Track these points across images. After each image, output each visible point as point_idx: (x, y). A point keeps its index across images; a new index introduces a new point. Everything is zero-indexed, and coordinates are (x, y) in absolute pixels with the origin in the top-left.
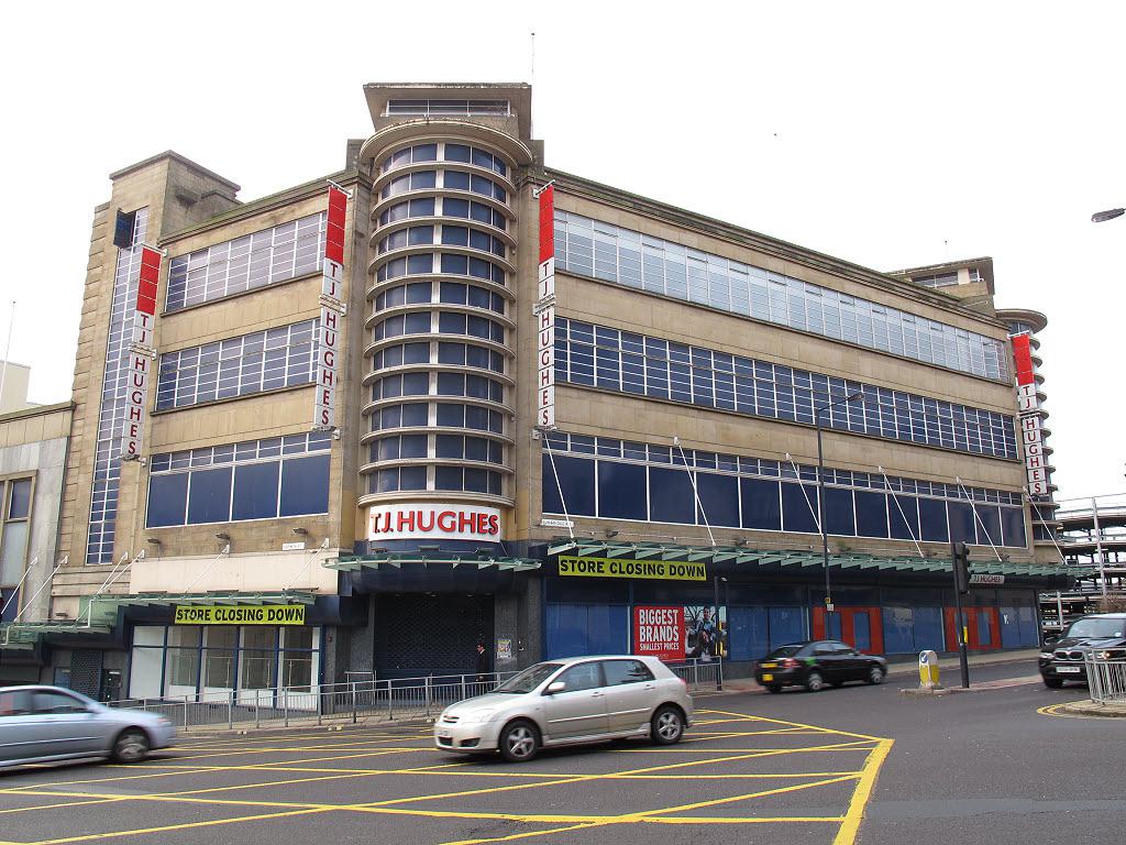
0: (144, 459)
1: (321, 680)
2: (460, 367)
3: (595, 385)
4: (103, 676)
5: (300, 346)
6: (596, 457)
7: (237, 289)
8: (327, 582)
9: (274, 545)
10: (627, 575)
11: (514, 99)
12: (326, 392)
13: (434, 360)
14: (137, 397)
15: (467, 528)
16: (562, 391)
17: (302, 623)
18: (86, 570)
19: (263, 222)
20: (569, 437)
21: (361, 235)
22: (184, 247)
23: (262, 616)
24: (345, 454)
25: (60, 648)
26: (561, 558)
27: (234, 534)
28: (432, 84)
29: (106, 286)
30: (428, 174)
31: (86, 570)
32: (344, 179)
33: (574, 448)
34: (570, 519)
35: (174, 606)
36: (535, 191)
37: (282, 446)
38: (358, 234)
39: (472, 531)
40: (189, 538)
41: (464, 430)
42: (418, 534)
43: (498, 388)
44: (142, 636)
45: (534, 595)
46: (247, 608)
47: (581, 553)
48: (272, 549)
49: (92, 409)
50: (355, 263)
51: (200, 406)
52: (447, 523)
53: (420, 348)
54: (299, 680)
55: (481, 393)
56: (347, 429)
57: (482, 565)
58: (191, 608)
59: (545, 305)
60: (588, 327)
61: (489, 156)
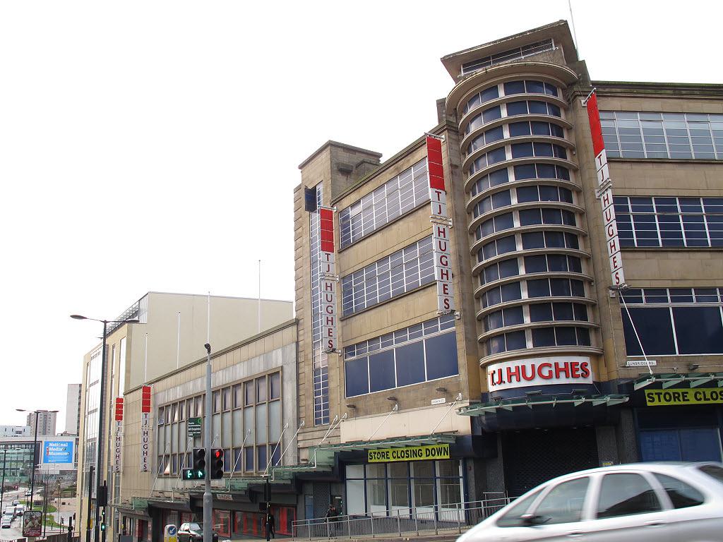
0: (340, 351)
1: (467, 499)
2: (540, 250)
3: (710, 246)
4: (332, 500)
5: (426, 255)
6: (670, 305)
7: (382, 223)
8: (463, 425)
9: (425, 403)
10: (712, 402)
11: (558, 34)
12: (444, 285)
13: (520, 248)
14: (330, 309)
15: (562, 374)
16: (629, 255)
17: (448, 457)
18: (315, 429)
19: (390, 174)
20: (642, 290)
21: (456, 167)
22: (346, 202)
23: (421, 454)
24: (466, 329)
25: (308, 482)
26: (647, 392)
27: (399, 397)
28: (490, 43)
29: (306, 239)
30: (495, 109)
31: (315, 429)
32: (438, 131)
33: (648, 300)
34: (649, 359)
35: (366, 450)
36: (583, 101)
37: (423, 329)
38: (453, 167)
39: (567, 376)
40: (372, 402)
41: (551, 298)
42: (524, 383)
43: (576, 262)
44: (352, 472)
45: (627, 421)
46: (412, 449)
47: (665, 386)
48: (424, 405)
49: (307, 323)
50: (454, 188)
51: (369, 309)
52: (545, 372)
53: (509, 240)
54: (452, 500)
55: (563, 266)
56: (464, 310)
57: (577, 403)
58: (377, 451)
59: (604, 188)
60: (647, 199)
61: (540, 84)
